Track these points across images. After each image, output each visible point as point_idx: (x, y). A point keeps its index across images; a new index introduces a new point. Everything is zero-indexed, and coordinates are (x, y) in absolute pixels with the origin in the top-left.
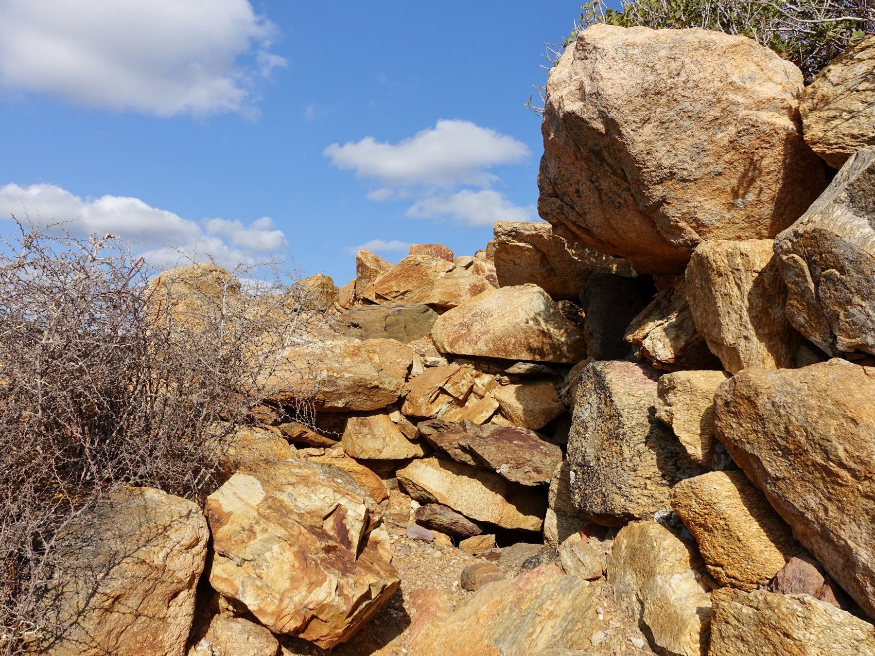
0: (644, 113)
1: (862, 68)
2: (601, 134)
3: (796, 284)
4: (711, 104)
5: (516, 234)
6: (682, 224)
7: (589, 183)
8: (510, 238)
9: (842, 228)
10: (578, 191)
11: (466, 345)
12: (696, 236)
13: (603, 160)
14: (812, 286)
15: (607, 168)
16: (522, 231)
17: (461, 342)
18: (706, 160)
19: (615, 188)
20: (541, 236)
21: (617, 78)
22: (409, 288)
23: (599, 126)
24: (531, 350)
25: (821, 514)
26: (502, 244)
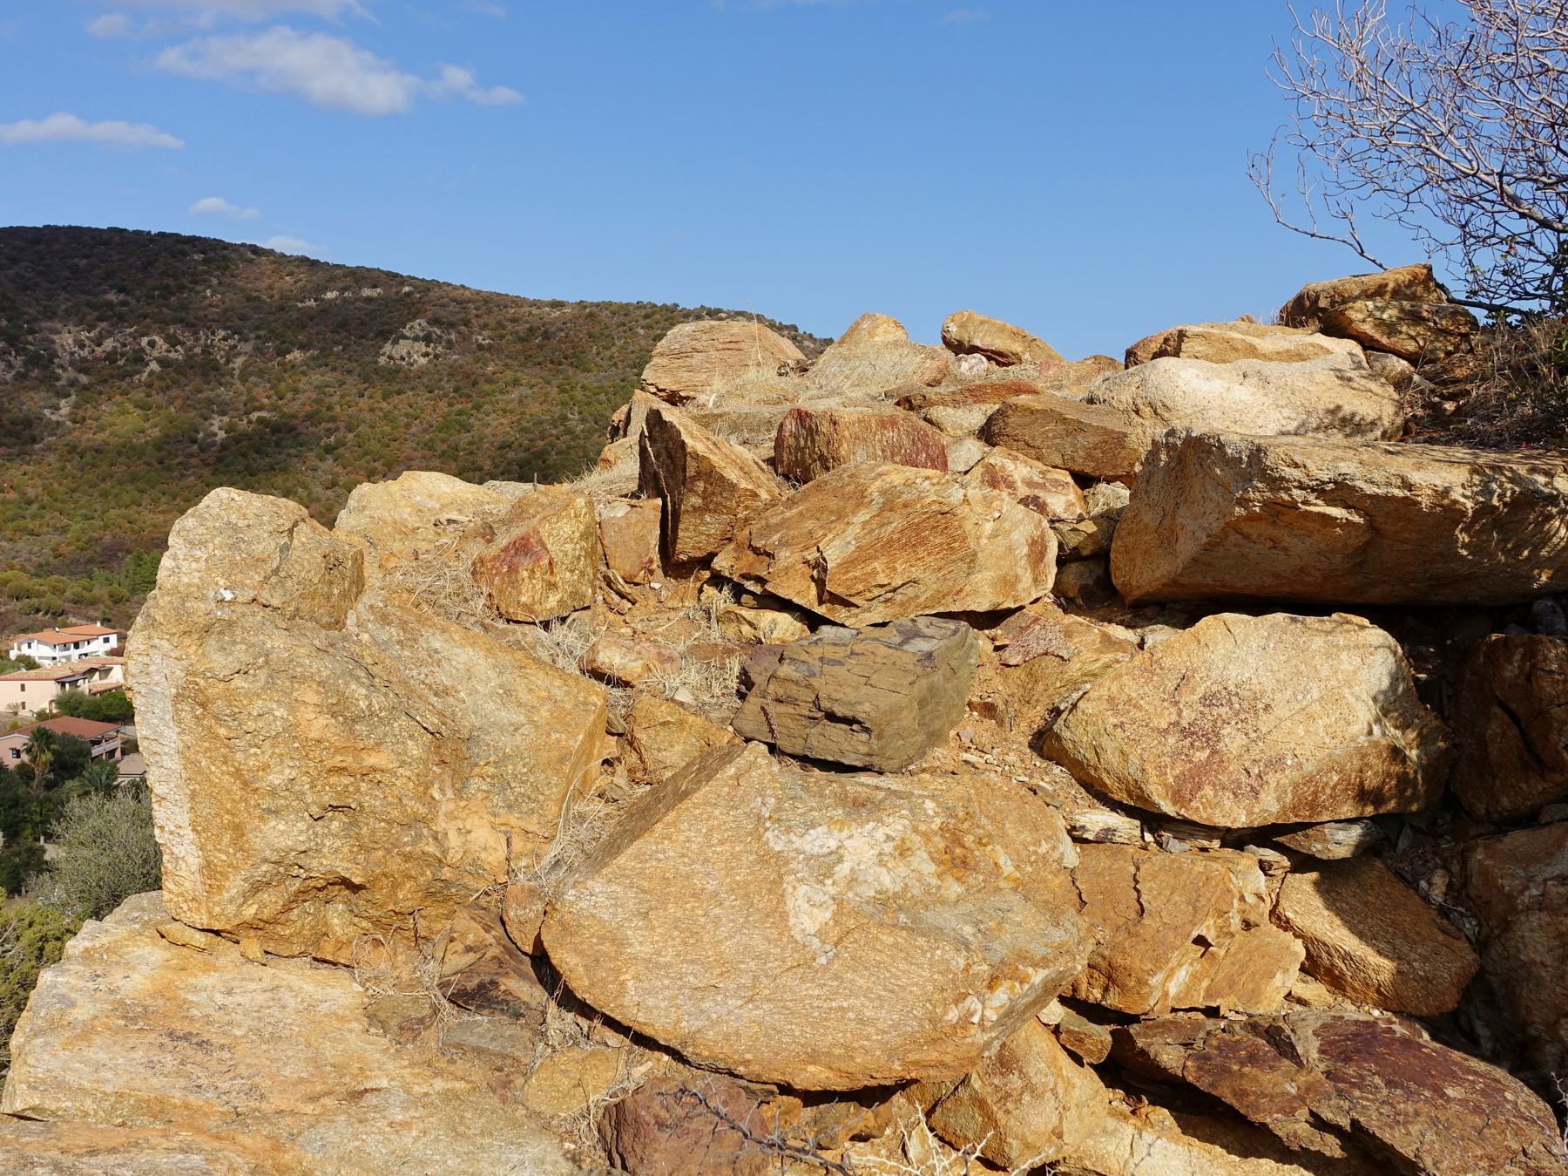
8: (1312, 498)
11: (1227, 801)
16: (1360, 484)
17: (1208, 791)
22: (916, 573)
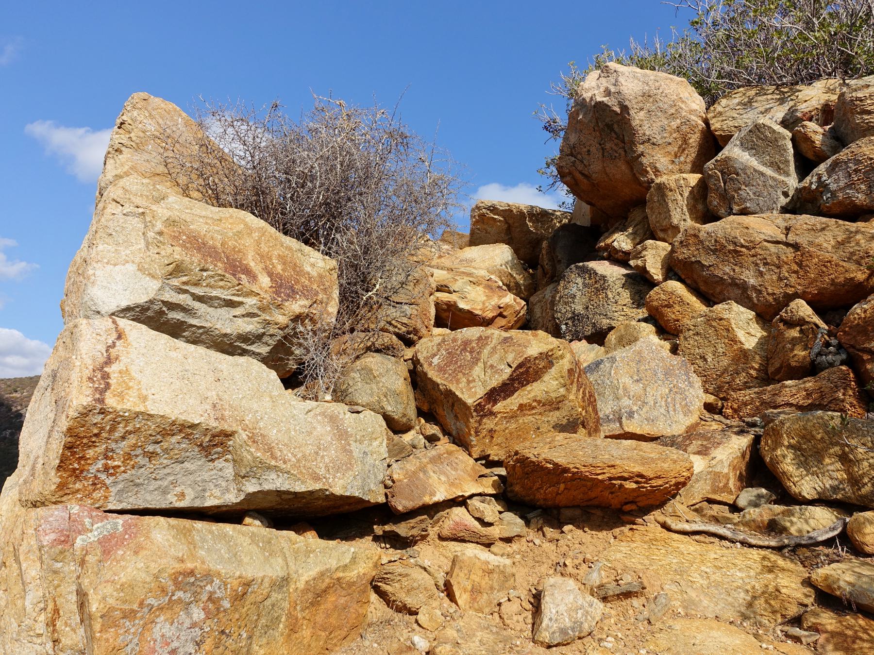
0: (641, 105)
1: (736, 101)
2: (617, 114)
3: (715, 185)
4: (671, 106)
5: (493, 209)
6: (648, 169)
7: (598, 145)
9: (738, 155)
10: (589, 151)
12: (654, 177)
13: (612, 130)
14: (723, 185)
18: (665, 135)
19: (615, 147)
21: (630, 86)
23: (618, 110)
25: (732, 273)
26: (483, 215)
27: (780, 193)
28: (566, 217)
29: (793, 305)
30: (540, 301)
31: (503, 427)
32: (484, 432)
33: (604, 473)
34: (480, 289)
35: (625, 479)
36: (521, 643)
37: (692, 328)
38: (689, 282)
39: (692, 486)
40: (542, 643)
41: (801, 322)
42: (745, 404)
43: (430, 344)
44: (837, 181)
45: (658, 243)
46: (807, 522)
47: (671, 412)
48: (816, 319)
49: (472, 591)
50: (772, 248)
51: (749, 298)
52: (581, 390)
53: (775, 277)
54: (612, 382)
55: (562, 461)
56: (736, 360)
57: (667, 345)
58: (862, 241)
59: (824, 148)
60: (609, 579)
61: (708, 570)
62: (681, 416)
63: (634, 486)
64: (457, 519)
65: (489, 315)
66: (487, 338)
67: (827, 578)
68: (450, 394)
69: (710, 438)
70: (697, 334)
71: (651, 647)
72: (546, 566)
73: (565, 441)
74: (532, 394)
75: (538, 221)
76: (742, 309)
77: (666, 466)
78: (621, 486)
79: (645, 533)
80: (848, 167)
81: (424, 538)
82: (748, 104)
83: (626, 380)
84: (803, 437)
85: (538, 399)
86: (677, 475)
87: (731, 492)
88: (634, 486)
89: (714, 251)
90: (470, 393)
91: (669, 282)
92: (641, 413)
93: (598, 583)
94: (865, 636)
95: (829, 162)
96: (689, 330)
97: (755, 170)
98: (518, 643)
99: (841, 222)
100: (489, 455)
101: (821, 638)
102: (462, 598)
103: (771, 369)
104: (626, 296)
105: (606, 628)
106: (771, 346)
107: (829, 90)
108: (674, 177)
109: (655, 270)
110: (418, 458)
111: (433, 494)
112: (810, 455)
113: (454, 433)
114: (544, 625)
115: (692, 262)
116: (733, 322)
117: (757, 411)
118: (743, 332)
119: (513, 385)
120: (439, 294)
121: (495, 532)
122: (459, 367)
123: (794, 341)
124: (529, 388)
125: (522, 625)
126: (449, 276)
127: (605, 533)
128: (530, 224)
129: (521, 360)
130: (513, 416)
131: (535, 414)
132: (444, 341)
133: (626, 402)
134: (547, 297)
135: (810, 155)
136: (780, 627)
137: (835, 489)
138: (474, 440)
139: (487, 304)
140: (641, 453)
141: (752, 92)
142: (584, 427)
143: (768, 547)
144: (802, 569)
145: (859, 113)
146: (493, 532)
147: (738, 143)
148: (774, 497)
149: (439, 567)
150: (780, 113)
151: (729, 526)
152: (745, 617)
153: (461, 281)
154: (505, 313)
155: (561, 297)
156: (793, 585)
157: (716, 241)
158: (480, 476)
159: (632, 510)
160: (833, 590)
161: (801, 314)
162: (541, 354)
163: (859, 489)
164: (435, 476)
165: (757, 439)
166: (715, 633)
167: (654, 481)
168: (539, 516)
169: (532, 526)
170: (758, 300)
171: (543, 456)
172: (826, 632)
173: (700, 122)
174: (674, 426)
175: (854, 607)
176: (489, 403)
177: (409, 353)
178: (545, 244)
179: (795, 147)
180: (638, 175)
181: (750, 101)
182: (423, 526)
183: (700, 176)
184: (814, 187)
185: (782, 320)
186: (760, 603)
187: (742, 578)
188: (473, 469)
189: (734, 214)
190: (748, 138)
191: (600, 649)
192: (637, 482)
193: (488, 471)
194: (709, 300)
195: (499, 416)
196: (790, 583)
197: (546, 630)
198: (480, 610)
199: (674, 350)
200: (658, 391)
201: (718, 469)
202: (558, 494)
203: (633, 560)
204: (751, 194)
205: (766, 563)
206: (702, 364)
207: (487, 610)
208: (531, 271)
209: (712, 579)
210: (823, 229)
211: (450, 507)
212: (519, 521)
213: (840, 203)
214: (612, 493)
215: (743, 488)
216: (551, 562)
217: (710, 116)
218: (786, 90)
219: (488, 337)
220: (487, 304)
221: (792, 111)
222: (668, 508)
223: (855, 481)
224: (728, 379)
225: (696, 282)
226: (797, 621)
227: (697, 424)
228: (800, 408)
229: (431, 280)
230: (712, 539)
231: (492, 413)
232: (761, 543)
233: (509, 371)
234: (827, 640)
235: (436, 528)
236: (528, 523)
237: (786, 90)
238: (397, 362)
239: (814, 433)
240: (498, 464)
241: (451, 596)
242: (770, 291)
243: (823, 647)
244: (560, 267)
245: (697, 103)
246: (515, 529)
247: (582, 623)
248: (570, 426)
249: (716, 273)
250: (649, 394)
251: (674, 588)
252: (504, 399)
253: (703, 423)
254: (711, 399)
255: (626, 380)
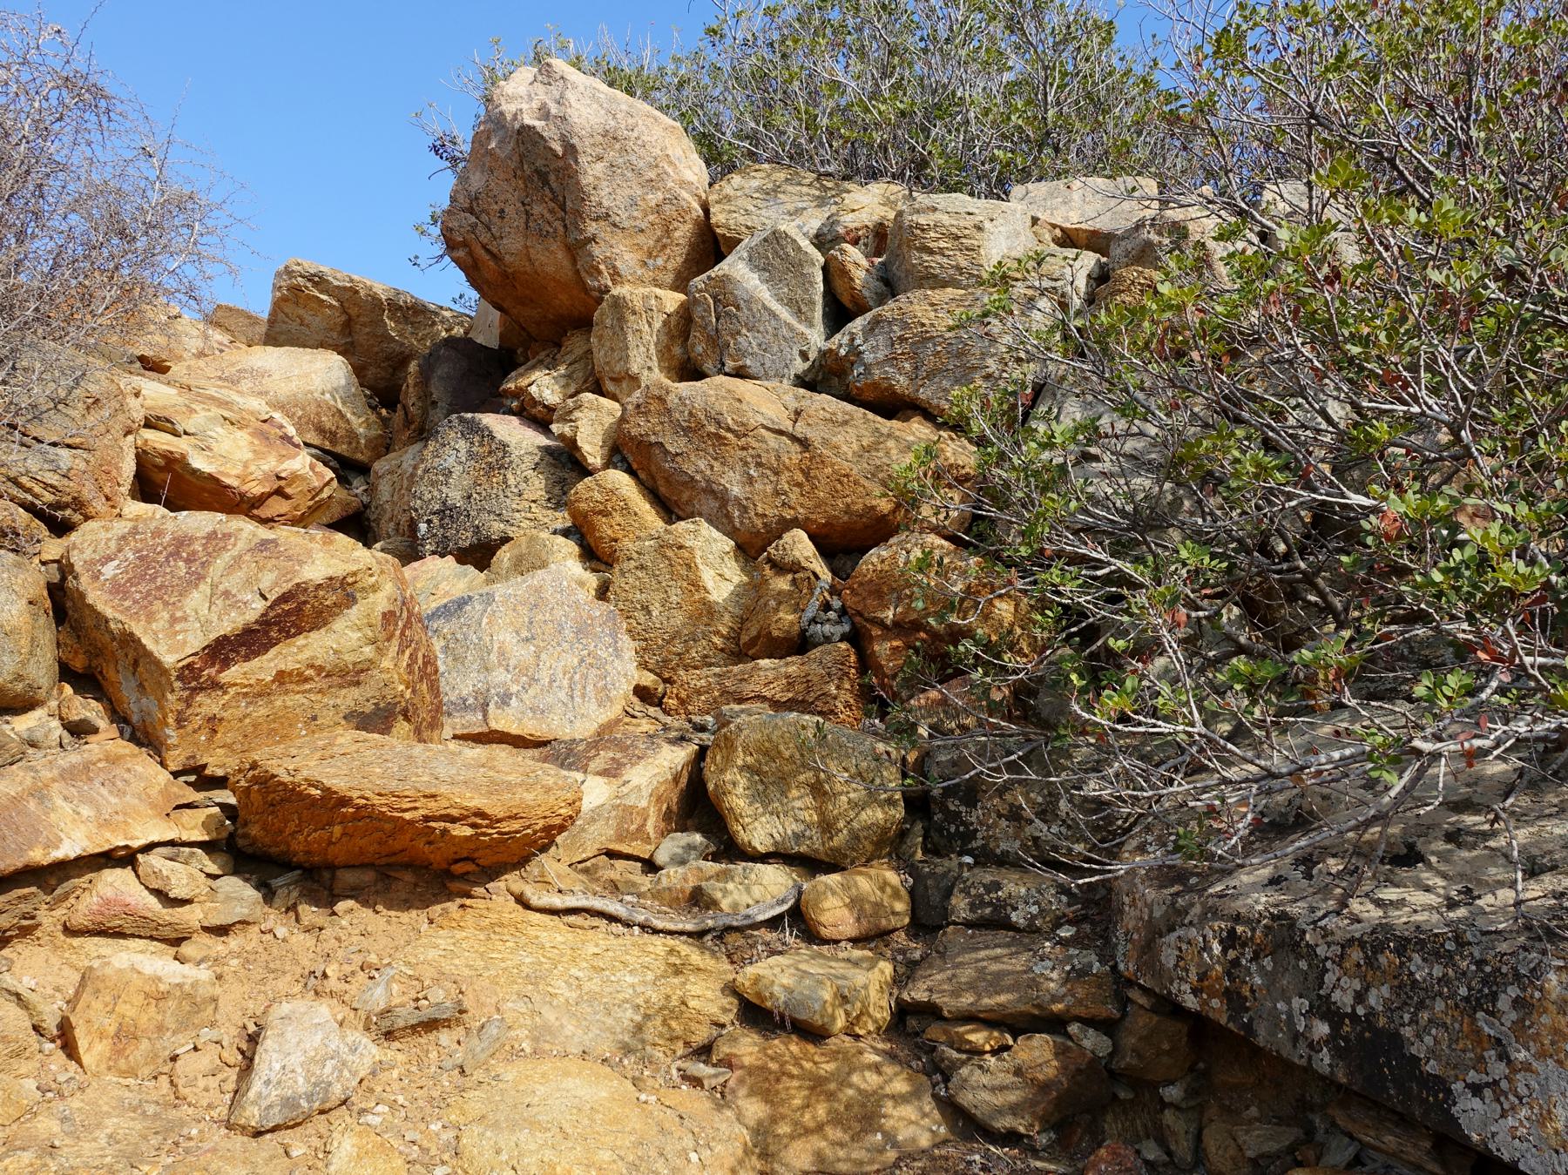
0: (599, 150)
1: (755, 183)
2: (557, 156)
3: (703, 318)
4: (650, 166)
5: (319, 281)
6: (602, 267)
8: (309, 285)
10: (502, 211)
13: (546, 182)
15: (547, 191)
18: (635, 214)
19: (548, 215)
20: (357, 292)
21: (585, 111)
24: (321, 430)
26: (296, 289)
27: (796, 352)
28: (461, 324)
29: (787, 537)
30: (391, 472)
31: (238, 713)
32: (198, 721)
33: (416, 808)
34: (243, 437)
35: (453, 820)
36: (201, 1131)
37: (635, 556)
38: (642, 476)
39: (583, 830)
40: (244, 1128)
41: (795, 568)
42: (699, 692)
43: (103, 535)
44: (874, 349)
45: (602, 399)
46: (748, 890)
47: (578, 700)
48: (819, 566)
49: (117, 1035)
50: (772, 441)
51: (728, 516)
52: (407, 653)
53: (769, 489)
54: (480, 639)
55: (339, 784)
56: (694, 618)
57: (592, 580)
58: (894, 452)
59: (866, 293)
60: (405, 999)
61: (580, 974)
62: (594, 706)
63: (468, 832)
64: (109, 893)
65: (256, 490)
66: (227, 536)
67: (757, 980)
68: (129, 641)
69: (628, 748)
70: (642, 567)
71: (453, 1117)
72: (288, 977)
73: (354, 748)
74: (307, 654)
75: (406, 319)
76: (716, 534)
77: (529, 797)
78: (445, 832)
79: (485, 913)
80: (892, 331)
81: (25, 932)
82: (772, 193)
83: (506, 637)
84: (766, 753)
85: (318, 663)
86: (548, 813)
87: (647, 840)
88: (468, 832)
89: (687, 431)
90: (172, 641)
91: (611, 472)
92: (525, 697)
93: (382, 1006)
94: (795, 1071)
95: (869, 316)
96: (629, 559)
97: (765, 308)
98: (194, 1132)
99: (870, 415)
100: (204, 766)
101: (733, 1078)
102: (92, 1050)
103: (745, 638)
104: (537, 486)
105: (379, 1089)
106: (752, 597)
107: (888, 202)
108: (642, 290)
109: (592, 449)
110: (32, 769)
111: (55, 843)
112: (770, 781)
113: (135, 719)
114: (251, 1094)
115: (651, 444)
116: (698, 553)
117: (713, 707)
118: (712, 572)
119: (266, 633)
120: (149, 434)
121: (191, 916)
122: (158, 589)
123: (781, 597)
124: (300, 641)
125: (213, 1095)
126: (180, 400)
127: (414, 913)
128: (391, 324)
129: (286, 587)
130: (262, 693)
131: (305, 691)
132: (134, 532)
133: (500, 676)
134: (405, 465)
135: (845, 299)
136: (679, 1063)
137: (798, 837)
138: (172, 734)
139: (253, 468)
140: (491, 773)
141: (781, 176)
142: (407, 719)
143: (681, 933)
144: (730, 967)
145: (917, 249)
146: (187, 917)
147: (745, 255)
148: (712, 849)
149: (57, 989)
150: (814, 222)
151: (628, 898)
152: (627, 1050)
153: (203, 414)
154: (288, 491)
155: (426, 471)
156: (709, 994)
157: (691, 414)
158: (178, 807)
159: (468, 873)
160: (763, 999)
161: (797, 553)
162: (331, 579)
163: (831, 838)
164: (67, 808)
165: (702, 752)
166: (569, 1083)
167: (504, 824)
168: (296, 882)
169: (278, 901)
170: (742, 523)
171: (305, 773)
172: (742, 1067)
173: (696, 205)
174: (578, 724)
175: (788, 1025)
176: (213, 665)
177: (53, 548)
178: (413, 367)
179: (826, 281)
180: (583, 274)
181: (776, 190)
182: (25, 907)
183: (682, 297)
184: (843, 352)
185: (769, 560)
186: (653, 1029)
187: (633, 986)
188: (164, 792)
189: (726, 374)
190: (761, 250)
191: (358, 1128)
192: (473, 826)
193: (198, 797)
194: (670, 510)
195: (232, 691)
196: (705, 996)
197: (254, 1103)
198: (131, 1072)
199: (602, 593)
200: (560, 661)
201: (630, 802)
202: (330, 843)
203: (457, 962)
204: (754, 344)
205: (673, 960)
206: (642, 619)
207: (146, 1071)
208: (384, 412)
209: (585, 989)
210: (846, 423)
211: (99, 868)
212: (250, 893)
213: (875, 385)
214: (430, 843)
215: (669, 832)
216: (299, 971)
217: (713, 198)
218: (830, 185)
219: (229, 535)
220: (253, 468)
221: (832, 221)
222: (533, 868)
223: (827, 827)
224: (679, 648)
225: (653, 478)
226: (704, 1052)
227: (618, 721)
228: (777, 705)
229: (132, 402)
230: (596, 921)
231: (215, 685)
232: (671, 926)
233: (259, 606)
234: (741, 1081)
235: (59, 912)
236: (269, 896)
237: (830, 185)
238: (18, 565)
239: (782, 748)
240: (220, 782)
241: (69, 1048)
242: (760, 511)
243: (733, 1091)
244: (436, 414)
245: (691, 169)
246: (238, 910)
247: (330, 1084)
248: (377, 719)
249: (684, 467)
250: (541, 659)
251: (522, 1007)
252: (247, 658)
253: (627, 720)
254: (648, 679)
255: (506, 637)
